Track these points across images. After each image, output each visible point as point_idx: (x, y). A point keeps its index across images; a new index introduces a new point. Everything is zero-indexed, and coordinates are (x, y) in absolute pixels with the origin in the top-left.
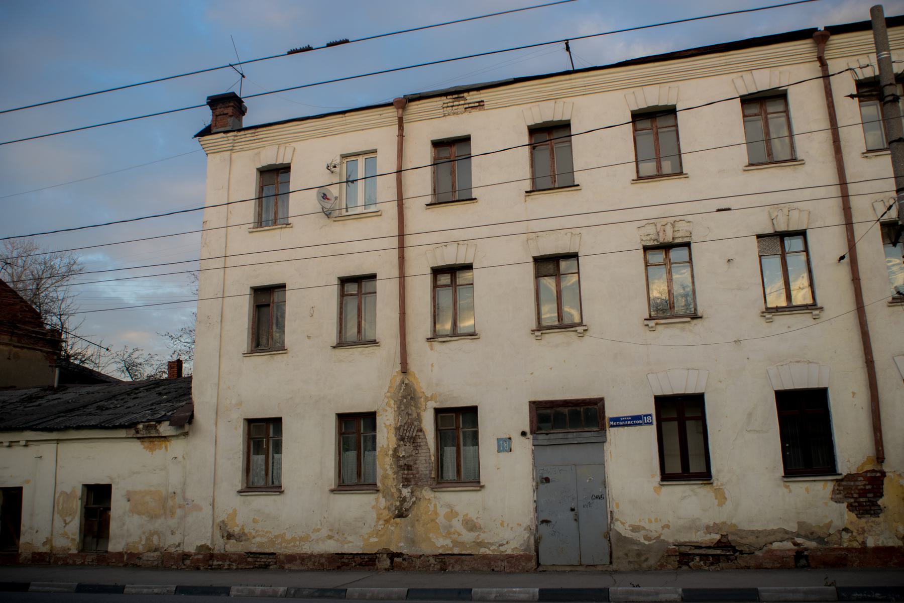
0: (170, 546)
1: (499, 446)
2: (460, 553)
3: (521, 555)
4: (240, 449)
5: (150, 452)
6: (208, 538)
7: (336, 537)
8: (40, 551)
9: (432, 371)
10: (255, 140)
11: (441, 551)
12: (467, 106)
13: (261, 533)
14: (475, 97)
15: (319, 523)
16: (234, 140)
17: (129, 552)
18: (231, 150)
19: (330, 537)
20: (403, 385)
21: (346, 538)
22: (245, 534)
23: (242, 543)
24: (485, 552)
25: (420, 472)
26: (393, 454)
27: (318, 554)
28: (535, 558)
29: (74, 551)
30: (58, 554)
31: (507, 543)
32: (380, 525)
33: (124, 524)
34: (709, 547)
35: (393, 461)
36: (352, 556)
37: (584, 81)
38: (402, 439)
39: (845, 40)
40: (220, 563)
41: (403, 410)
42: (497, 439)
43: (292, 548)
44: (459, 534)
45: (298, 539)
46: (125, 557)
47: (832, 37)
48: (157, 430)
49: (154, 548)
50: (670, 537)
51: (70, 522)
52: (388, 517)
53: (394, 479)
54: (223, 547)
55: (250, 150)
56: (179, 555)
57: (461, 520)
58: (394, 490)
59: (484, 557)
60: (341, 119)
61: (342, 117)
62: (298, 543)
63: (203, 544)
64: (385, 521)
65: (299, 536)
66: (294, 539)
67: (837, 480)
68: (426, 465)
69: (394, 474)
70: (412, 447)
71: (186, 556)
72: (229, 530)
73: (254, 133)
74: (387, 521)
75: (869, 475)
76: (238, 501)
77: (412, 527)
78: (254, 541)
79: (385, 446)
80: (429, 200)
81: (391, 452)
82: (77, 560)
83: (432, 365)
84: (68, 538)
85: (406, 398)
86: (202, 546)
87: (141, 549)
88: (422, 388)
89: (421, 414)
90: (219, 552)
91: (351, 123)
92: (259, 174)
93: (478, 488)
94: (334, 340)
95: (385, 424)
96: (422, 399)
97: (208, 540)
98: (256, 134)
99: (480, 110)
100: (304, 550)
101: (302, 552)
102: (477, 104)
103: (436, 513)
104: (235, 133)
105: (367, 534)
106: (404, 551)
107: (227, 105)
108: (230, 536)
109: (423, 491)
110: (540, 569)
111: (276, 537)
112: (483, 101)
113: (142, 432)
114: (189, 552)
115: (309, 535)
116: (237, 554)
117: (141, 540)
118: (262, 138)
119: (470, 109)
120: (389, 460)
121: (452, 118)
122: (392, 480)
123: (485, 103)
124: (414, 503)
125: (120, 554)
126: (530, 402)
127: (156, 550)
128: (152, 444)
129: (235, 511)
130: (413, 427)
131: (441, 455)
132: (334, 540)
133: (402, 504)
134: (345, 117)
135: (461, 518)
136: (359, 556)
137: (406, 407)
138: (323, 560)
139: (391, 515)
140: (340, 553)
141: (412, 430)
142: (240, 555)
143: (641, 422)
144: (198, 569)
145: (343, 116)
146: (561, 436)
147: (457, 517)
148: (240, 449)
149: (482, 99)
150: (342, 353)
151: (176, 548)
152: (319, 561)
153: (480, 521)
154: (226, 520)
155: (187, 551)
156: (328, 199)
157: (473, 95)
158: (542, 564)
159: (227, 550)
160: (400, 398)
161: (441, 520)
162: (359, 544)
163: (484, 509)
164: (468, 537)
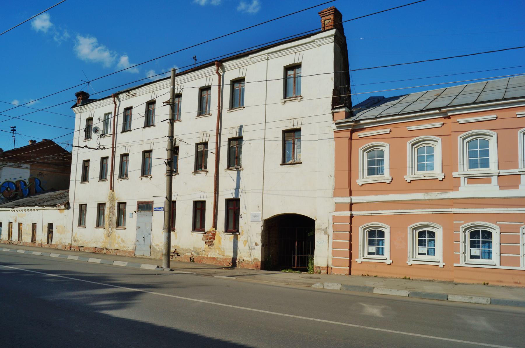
12: (132, 95)
112: (135, 94)
164: (122, 245)
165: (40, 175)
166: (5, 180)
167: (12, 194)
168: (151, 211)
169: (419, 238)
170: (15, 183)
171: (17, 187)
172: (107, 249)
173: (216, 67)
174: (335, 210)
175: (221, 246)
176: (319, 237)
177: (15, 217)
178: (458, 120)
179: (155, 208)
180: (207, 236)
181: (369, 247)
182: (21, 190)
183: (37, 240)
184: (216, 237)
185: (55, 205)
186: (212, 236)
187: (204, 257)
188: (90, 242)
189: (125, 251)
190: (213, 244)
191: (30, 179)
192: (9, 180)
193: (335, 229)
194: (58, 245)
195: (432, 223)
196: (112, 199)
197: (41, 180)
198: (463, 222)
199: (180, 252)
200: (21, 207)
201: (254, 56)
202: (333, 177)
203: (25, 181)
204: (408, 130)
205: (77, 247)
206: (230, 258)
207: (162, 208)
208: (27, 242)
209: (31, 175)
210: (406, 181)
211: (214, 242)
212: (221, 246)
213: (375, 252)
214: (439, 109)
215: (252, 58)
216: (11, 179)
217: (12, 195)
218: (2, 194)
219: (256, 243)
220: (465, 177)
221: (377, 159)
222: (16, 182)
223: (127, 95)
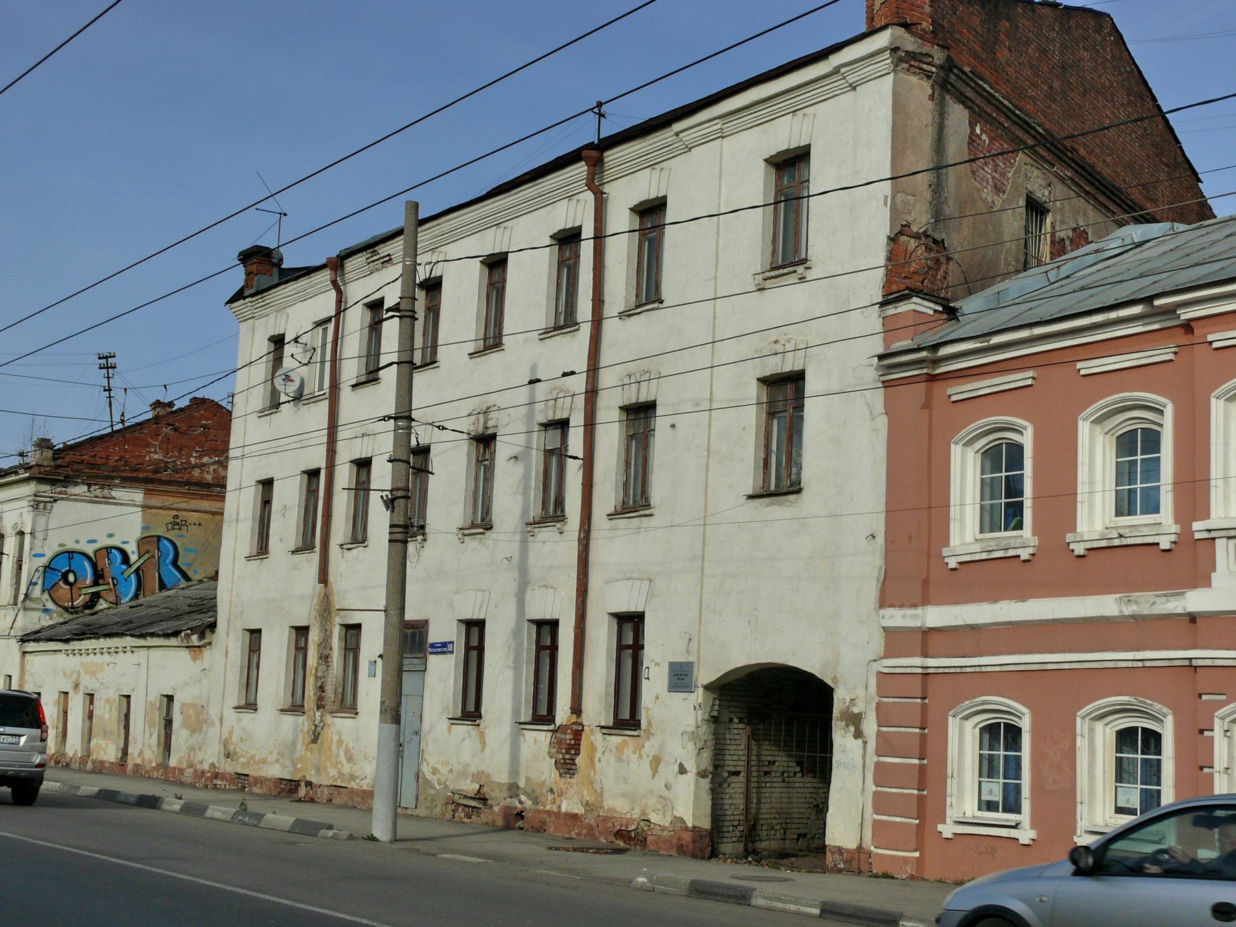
12: (382, 261)
18: (253, 317)
38: (321, 658)
39: (547, 188)
47: (606, 154)
80: (471, 347)
92: (487, 271)
93: (353, 715)
112: (389, 255)
156: (292, 381)
157: (382, 248)
164: (347, 768)
165: (177, 527)
166: (60, 545)
167: (80, 595)
168: (422, 655)
169: (1117, 752)
170: (92, 555)
171: (99, 569)
172: (309, 784)
173: (586, 168)
174: (882, 654)
175: (595, 774)
176: (844, 745)
177: (75, 676)
178: (1210, 338)
179: (432, 646)
180: (560, 742)
181: (983, 784)
182: (113, 579)
183: (132, 754)
184: (582, 742)
185: (176, 634)
186: (573, 742)
187: (549, 813)
188: (264, 761)
189: (352, 790)
190: (573, 767)
191: (141, 542)
192: (71, 545)
193: (883, 717)
194: (184, 769)
195: (1141, 702)
196: (326, 608)
197: (178, 544)
198: (1224, 697)
199: (493, 794)
200: (90, 638)
201: (687, 127)
202: (881, 539)
203: (124, 547)
204: (1083, 373)
205: (231, 775)
206: (614, 815)
207: (450, 643)
208: (105, 759)
209: (145, 528)
210: (1073, 551)
211: (577, 762)
212: (595, 774)
213: (996, 799)
214: (1149, 300)
215: (681, 132)
216: (77, 542)
217: (83, 596)
218: (50, 595)
219: (681, 765)
220: (1229, 538)
221: (1137, 455)
222: (96, 552)
223: (368, 261)
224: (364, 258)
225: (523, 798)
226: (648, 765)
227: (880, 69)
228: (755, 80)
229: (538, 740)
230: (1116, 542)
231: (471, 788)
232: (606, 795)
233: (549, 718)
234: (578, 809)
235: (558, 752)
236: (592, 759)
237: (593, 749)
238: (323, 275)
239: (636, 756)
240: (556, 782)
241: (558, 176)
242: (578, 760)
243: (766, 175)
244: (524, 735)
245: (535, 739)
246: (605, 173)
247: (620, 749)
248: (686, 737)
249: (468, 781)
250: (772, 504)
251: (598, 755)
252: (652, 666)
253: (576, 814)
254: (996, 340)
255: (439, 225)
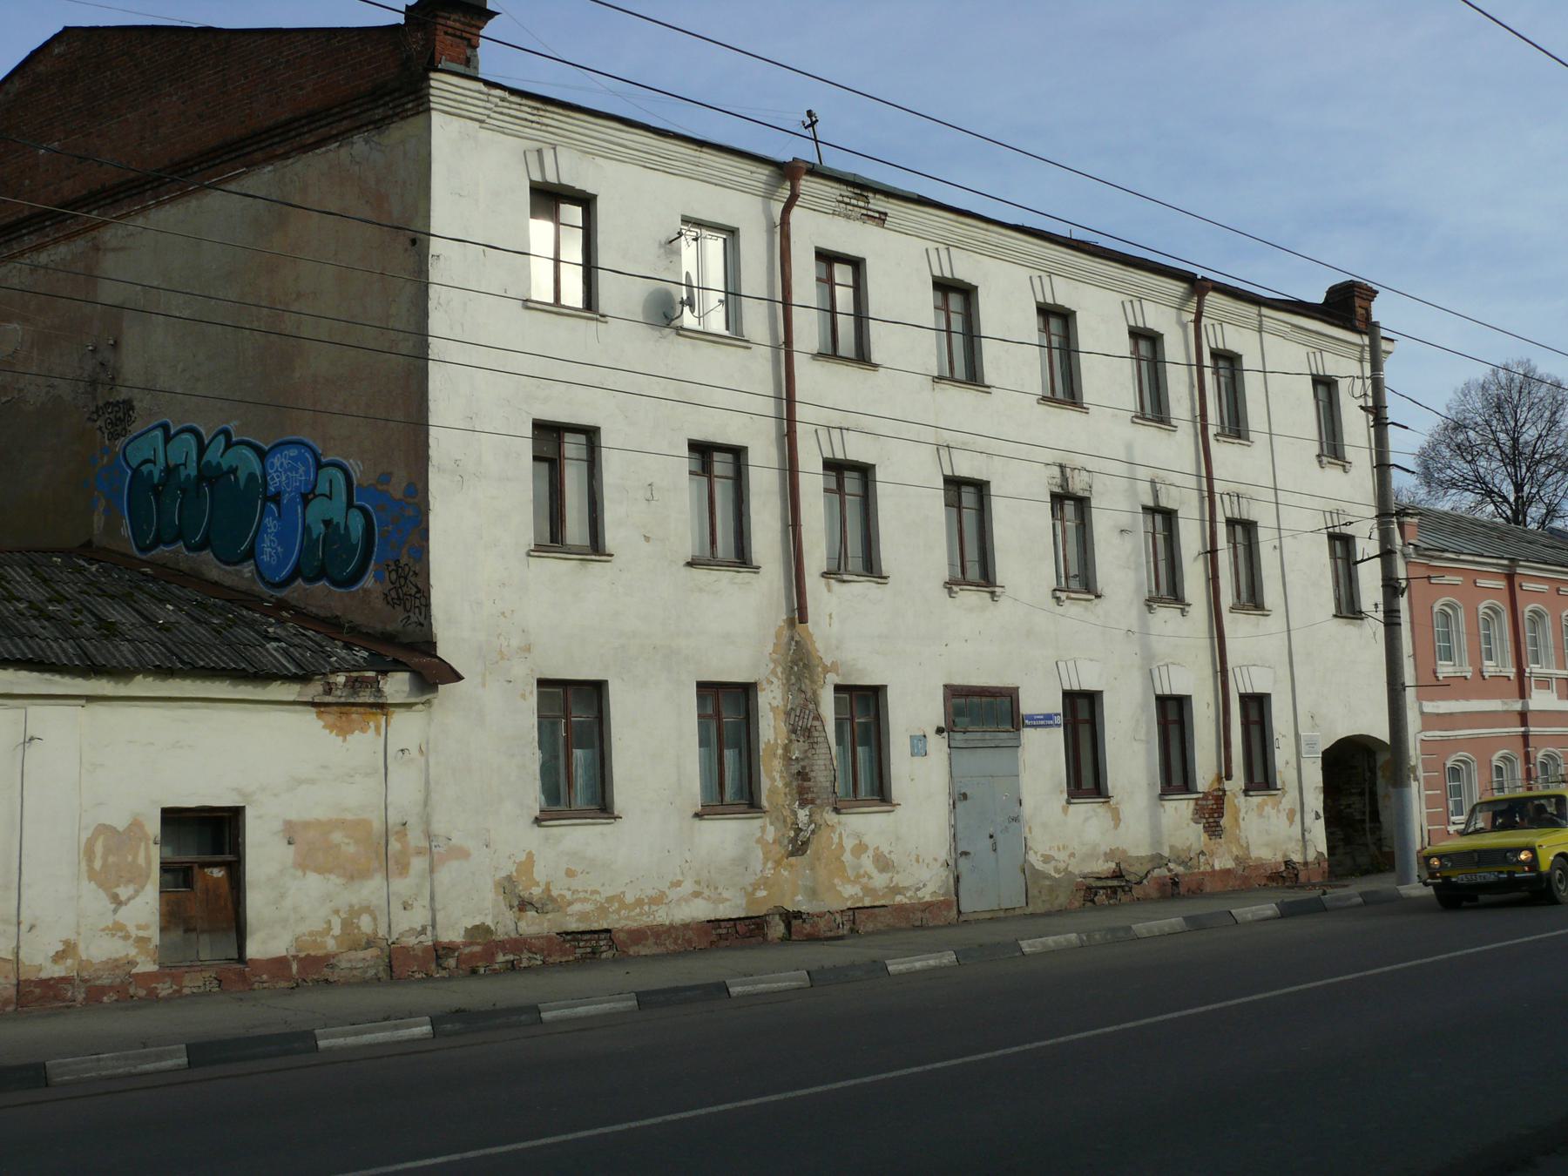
0: (402, 935)
1: (912, 746)
2: (873, 904)
3: (941, 901)
4: (534, 737)
5: (337, 735)
6: (487, 911)
7: (707, 893)
8: (44, 975)
9: (830, 625)
10: (532, 122)
11: (849, 904)
12: (865, 212)
13: (582, 895)
14: (880, 203)
15: (678, 871)
16: (497, 106)
17: (302, 955)
18: (482, 122)
19: (697, 894)
20: (793, 643)
21: (720, 894)
22: (552, 899)
23: (549, 916)
24: (901, 900)
25: (819, 785)
26: (783, 755)
27: (682, 925)
28: (955, 903)
29: (147, 966)
30: (99, 978)
31: (924, 885)
32: (769, 869)
33: (282, 896)
34: (1107, 878)
35: (783, 765)
36: (732, 923)
37: (999, 239)
38: (794, 731)
40: (511, 957)
41: (793, 684)
42: (911, 736)
43: (638, 918)
44: (870, 878)
45: (646, 901)
46: (295, 967)
48: (379, 690)
49: (364, 941)
50: (1076, 868)
51: (129, 899)
52: (780, 855)
53: (785, 794)
54: (512, 927)
55: (515, 136)
56: (426, 949)
57: (871, 856)
58: (787, 813)
59: (901, 908)
60: (692, 153)
61: (696, 150)
62: (646, 908)
63: (478, 923)
64: (775, 862)
65: (647, 896)
66: (639, 902)
67: (1197, 799)
68: (825, 773)
69: (786, 788)
70: (806, 744)
71: (440, 952)
72: (522, 894)
73: (538, 109)
74: (778, 863)
75: (1215, 793)
76: (534, 838)
77: (811, 869)
78: (570, 910)
79: (772, 742)
81: (780, 752)
82: (160, 986)
83: (830, 615)
84: (127, 937)
85: (797, 665)
86: (476, 927)
87: (331, 945)
88: (818, 651)
89: (818, 692)
90: (506, 937)
91: (706, 166)
94: (688, 549)
95: (770, 704)
96: (820, 669)
97: (486, 915)
98: (542, 113)
99: (877, 225)
100: (658, 919)
101: (655, 923)
102: (877, 215)
103: (841, 846)
104: (506, 95)
105: (751, 884)
106: (804, 908)
107: (473, 22)
108: (524, 905)
109: (824, 814)
110: (962, 918)
111: (610, 900)
112: (886, 214)
113: (339, 693)
114: (451, 942)
115: (664, 893)
116: (542, 938)
117: (330, 928)
118: (547, 125)
119: (866, 218)
120: (777, 764)
121: (841, 221)
122: (783, 795)
123: (888, 218)
124: (813, 832)
125: (280, 963)
126: (946, 686)
127: (370, 943)
128: (344, 719)
129: (530, 856)
130: (807, 712)
131: (557, 758)
132: (703, 898)
133: (797, 835)
134: (701, 151)
135: (871, 852)
136: (742, 922)
137: (799, 679)
138: (690, 934)
139: (783, 852)
140: (713, 919)
141: (806, 717)
142: (549, 939)
143: (1052, 722)
144: (474, 972)
145: (699, 149)
146: (979, 735)
147: (866, 852)
148: (534, 737)
149: (887, 211)
150: (700, 574)
151: (417, 937)
152: (684, 935)
153: (893, 857)
154: (515, 874)
155: (447, 940)
157: (879, 200)
158: (962, 911)
159: (521, 931)
160: (790, 664)
161: (847, 857)
162: (739, 902)
163: (898, 838)
164: (880, 880)
186: (1215, 807)
187: (1203, 873)
190: (1218, 829)
212: (1240, 832)
224: (838, 192)
225: (1172, 866)
226: (1285, 817)
227: (469, 100)
228: (1039, 233)
229: (1180, 809)
230: (1498, 674)
231: (1105, 868)
232: (1252, 848)
233: (1187, 785)
234: (1230, 864)
235: (1201, 817)
236: (1236, 820)
237: (1237, 811)
238: (738, 165)
239: (1275, 811)
240: (1205, 845)
241: (1167, 283)
242: (1223, 822)
243: (1038, 320)
244: (1163, 806)
245: (1176, 808)
246: (1190, 303)
247: (1260, 807)
248: (1317, 791)
249: (1100, 861)
250: (1349, 624)
251: (1242, 815)
252: (1280, 737)
253: (1229, 870)
254: (1462, 557)
255: (987, 230)
